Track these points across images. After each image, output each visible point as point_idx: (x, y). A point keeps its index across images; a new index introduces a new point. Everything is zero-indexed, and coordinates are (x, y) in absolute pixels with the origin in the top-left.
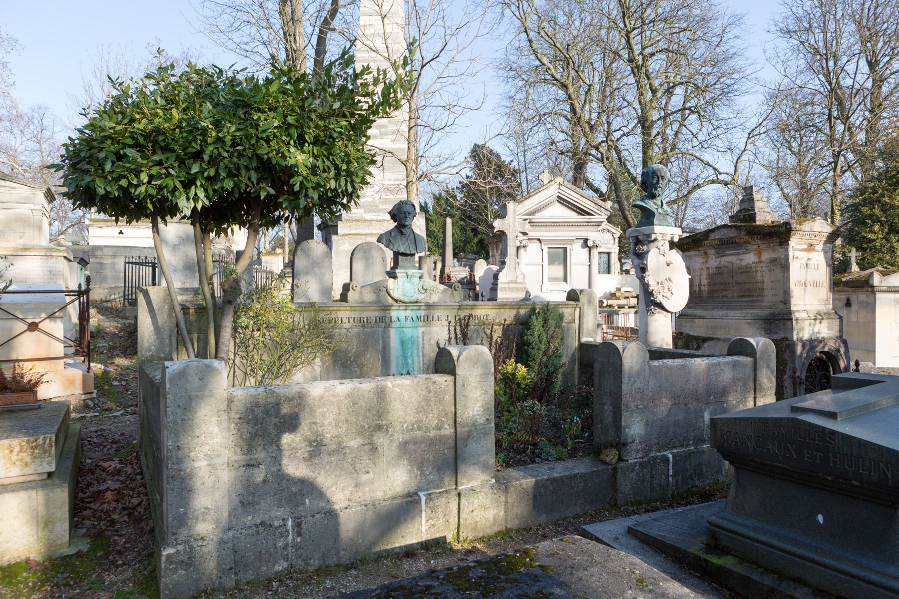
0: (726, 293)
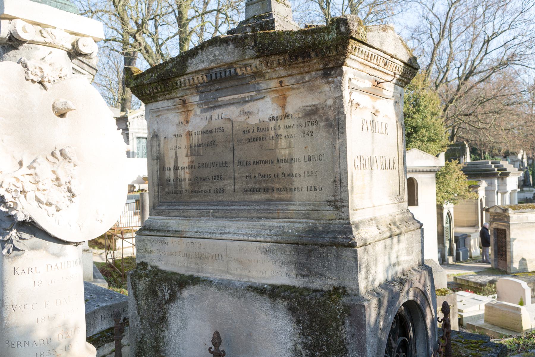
0: (220, 184)
